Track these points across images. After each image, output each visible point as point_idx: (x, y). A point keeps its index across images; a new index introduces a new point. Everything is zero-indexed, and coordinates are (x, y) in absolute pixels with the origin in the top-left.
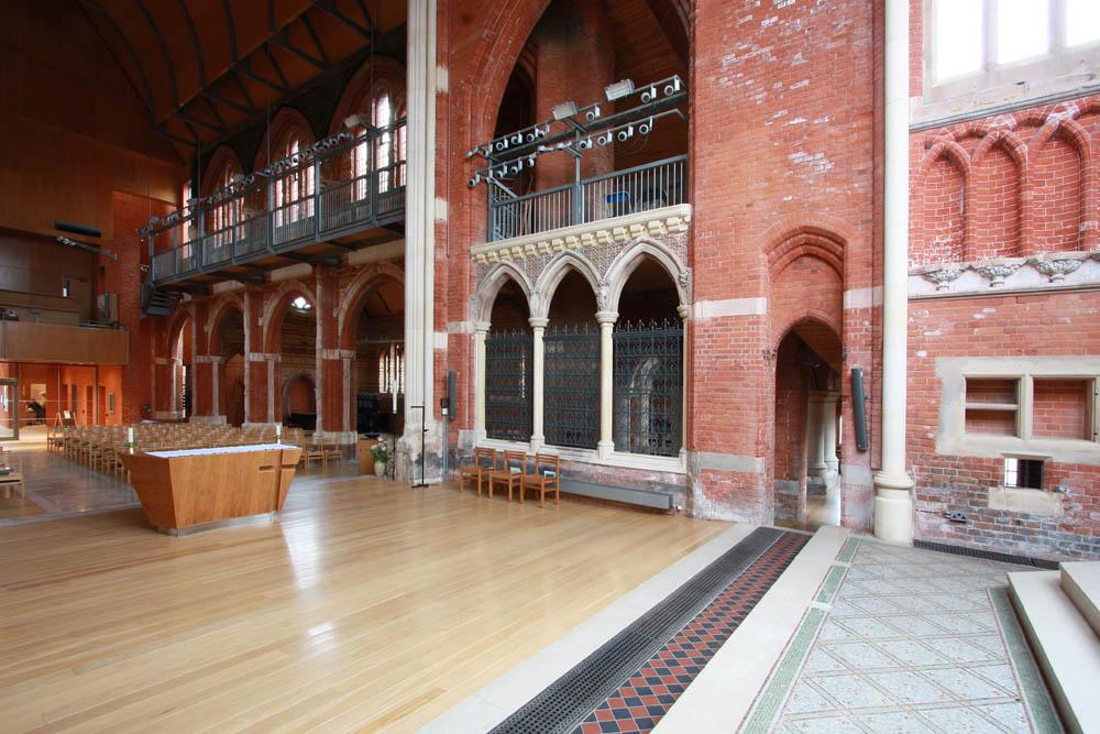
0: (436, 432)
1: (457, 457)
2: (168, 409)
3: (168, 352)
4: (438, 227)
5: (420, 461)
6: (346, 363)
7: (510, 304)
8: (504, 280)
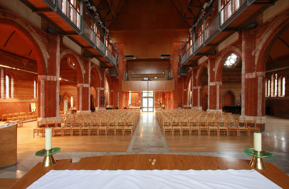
2: (186, 104)
3: (186, 87)
6: (218, 87)
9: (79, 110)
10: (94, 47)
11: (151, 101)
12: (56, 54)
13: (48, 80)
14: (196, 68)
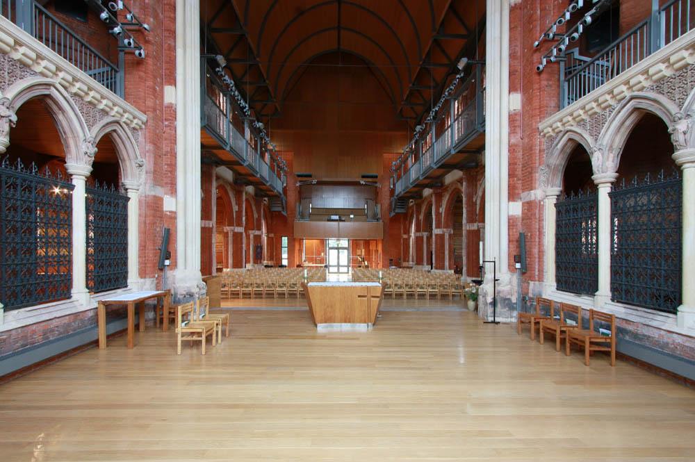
0: (510, 282)
1: (528, 304)
2: (408, 261)
3: (407, 232)
4: (512, 118)
5: (494, 303)
6: (447, 237)
7: (577, 171)
8: (570, 144)
9: (227, 267)
10: (226, 146)
11: (344, 255)
12: (211, 191)
13: (286, 238)
14: (419, 201)
